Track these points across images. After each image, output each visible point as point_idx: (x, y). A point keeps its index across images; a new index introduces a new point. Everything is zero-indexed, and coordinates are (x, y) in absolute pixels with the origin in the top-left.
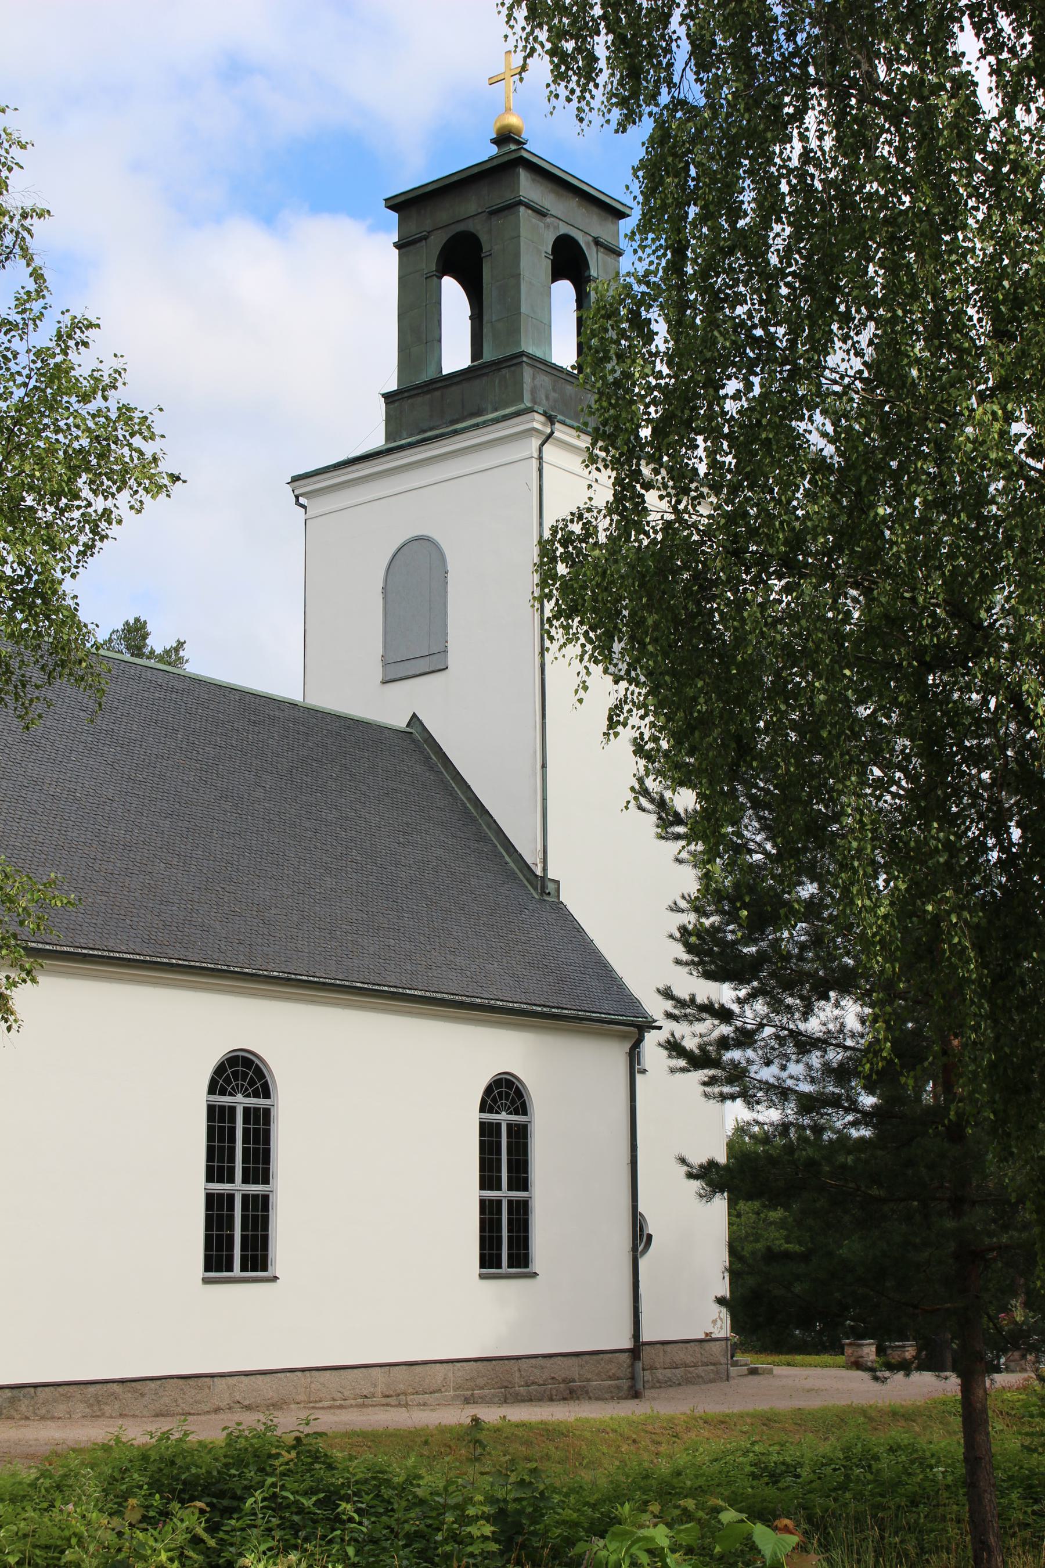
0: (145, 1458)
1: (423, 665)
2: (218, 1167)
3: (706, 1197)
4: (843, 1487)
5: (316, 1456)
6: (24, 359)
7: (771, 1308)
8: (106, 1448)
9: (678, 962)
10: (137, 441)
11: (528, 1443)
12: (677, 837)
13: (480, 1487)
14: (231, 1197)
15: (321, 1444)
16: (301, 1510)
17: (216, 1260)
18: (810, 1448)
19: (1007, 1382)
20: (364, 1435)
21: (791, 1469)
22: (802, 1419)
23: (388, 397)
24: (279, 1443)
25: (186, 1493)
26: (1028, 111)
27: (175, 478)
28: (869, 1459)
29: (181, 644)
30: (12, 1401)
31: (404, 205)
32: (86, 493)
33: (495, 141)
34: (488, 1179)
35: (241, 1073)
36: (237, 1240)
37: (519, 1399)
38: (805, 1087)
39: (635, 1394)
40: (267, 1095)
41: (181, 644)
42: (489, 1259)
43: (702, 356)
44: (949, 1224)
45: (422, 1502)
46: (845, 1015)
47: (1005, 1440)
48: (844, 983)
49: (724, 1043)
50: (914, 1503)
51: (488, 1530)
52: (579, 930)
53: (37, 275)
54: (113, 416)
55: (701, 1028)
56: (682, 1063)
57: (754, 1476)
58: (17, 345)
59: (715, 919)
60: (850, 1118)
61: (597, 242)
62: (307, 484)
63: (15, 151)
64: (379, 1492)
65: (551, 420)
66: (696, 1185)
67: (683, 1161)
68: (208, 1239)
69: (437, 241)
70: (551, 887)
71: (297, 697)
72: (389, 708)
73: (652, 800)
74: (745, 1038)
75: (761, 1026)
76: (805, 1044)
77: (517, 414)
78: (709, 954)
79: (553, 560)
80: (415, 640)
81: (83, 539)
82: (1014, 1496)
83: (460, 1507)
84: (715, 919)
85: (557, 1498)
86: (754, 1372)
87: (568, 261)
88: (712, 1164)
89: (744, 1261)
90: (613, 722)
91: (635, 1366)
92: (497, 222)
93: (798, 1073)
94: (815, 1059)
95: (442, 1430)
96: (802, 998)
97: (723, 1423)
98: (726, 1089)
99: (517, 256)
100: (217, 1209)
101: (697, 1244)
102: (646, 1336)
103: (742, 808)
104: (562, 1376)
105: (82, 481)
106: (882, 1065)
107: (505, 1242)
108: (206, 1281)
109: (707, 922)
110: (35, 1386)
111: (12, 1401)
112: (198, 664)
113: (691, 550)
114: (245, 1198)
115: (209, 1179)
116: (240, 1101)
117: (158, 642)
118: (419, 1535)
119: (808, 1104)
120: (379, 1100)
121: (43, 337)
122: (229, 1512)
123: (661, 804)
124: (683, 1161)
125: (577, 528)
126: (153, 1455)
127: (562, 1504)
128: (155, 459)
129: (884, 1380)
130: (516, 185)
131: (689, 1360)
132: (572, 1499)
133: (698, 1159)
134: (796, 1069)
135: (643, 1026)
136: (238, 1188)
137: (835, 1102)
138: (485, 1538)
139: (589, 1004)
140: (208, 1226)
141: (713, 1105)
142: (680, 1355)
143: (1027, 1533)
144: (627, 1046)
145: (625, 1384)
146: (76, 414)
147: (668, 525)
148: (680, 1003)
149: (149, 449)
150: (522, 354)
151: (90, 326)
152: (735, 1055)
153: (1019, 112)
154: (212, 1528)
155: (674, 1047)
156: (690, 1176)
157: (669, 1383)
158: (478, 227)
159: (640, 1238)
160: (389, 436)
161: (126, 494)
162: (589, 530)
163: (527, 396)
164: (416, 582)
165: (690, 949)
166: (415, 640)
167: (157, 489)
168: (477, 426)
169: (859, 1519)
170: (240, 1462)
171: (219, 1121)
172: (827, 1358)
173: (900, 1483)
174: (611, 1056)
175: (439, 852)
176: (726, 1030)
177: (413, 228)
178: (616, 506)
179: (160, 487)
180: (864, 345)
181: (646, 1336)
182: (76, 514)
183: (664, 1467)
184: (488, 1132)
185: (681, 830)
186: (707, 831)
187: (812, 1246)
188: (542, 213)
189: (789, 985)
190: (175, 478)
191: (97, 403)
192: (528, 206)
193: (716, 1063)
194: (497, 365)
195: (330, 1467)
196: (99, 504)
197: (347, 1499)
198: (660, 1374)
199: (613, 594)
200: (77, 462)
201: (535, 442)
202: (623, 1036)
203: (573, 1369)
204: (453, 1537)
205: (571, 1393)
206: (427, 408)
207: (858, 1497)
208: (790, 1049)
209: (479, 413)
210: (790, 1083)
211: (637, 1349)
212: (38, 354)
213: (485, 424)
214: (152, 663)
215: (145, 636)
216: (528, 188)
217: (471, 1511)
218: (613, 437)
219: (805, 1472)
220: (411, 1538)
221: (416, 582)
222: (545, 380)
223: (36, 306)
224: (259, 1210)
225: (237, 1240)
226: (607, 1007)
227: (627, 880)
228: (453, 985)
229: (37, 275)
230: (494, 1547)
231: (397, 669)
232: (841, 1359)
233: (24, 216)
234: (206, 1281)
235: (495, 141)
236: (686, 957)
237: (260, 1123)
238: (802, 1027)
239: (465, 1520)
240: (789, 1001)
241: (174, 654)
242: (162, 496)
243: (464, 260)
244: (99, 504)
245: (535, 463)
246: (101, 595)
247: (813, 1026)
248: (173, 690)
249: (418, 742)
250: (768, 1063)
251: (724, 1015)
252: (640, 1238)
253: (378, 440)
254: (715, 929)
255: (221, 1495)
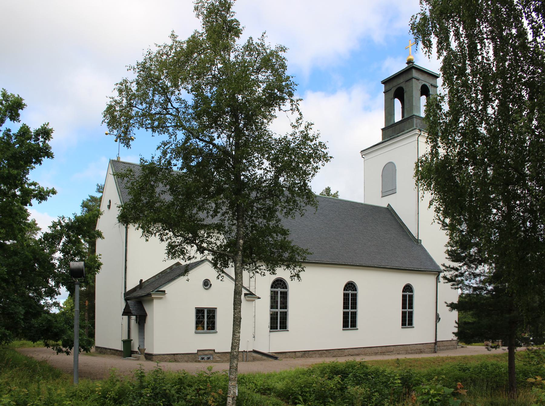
0: (329, 366)
1: (391, 192)
2: (346, 306)
3: (451, 311)
4: (480, 373)
5: (364, 366)
6: (298, 134)
7: (465, 334)
8: (321, 364)
9: (446, 258)
10: (323, 150)
11: (410, 363)
12: (447, 229)
13: (398, 372)
14: (348, 312)
15: (365, 364)
16: (360, 377)
17: (345, 325)
18: (473, 364)
19: (521, 350)
20: (376, 361)
21: (468, 369)
22: (472, 357)
23: (383, 130)
24: (356, 363)
25: (337, 373)
26: (540, 38)
27: (331, 157)
28: (486, 367)
29: (338, 192)
30: (304, 354)
31: (385, 82)
32: (312, 163)
33: (407, 63)
34: (404, 307)
35: (350, 286)
36: (350, 321)
37: (409, 353)
38: (475, 285)
39: (435, 352)
40: (356, 290)
41: (338, 192)
42: (404, 324)
43: (456, 110)
44: (507, 316)
45: (386, 376)
46: (484, 268)
47: (518, 363)
48: (485, 261)
49: (456, 276)
50: (496, 376)
51: (399, 381)
52: (426, 251)
53: (301, 114)
54: (318, 144)
55: (451, 273)
56: (446, 281)
57: (460, 370)
58: (297, 131)
59: (455, 248)
60: (485, 292)
61: (432, 85)
62: (365, 152)
63: (295, 86)
64: (377, 373)
65: (420, 131)
66: (449, 308)
67: (446, 303)
68: (344, 321)
69: (393, 90)
70: (419, 241)
71: (362, 202)
72: (383, 203)
73: (441, 221)
74: (462, 275)
75: (465, 272)
76: (475, 276)
77: (412, 130)
78: (454, 256)
79: (418, 167)
80: (389, 188)
81: (312, 173)
82: (521, 375)
83: (393, 377)
84: (455, 248)
85: (415, 375)
86: (462, 347)
87: (425, 91)
88: (452, 303)
89: (461, 324)
90: (431, 204)
91: (436, 346)
92: (408, 83)
93: (474, 283)
94: (478, 279)
95: (392, 360)
96: (475, 265)
97: (454, 358)
98: (456, 287)
99: (412, 91)
100: (345, 315)
101: (450, 321)
102: (438, 340)
103: (463, 222)
104: (419, 348)
105: (311, 160)
106: (493, 279)
107: (407, 320)
108: (343, 330)
109: (453, 249)
110: (309, 351)
111: (304, 354)
112: (341, 197)
113: (450, 163)
114: (351, 312)
115: (344, 309)
116: (350, 292)
117: (333, 192)
118: (385, 382)
119: (475, 289)
120: (380, 291)
121: (302, 128)
122: (346, 377)
123: (443, 222)
124: (446, 303)
125: (424, 159)
126: (331, 366)
127: (416, 376)
128: (327, 153)
129: (490, 350)
130: (412, 74)
131: (448, 345)
132: (419, 375)
133: (449, 302)
134: (473, 281)
135: (439, 272)
136: (350, 310)
137: (482, 288)
138: (399, 383)
139: (428, 268)
140: (344, 318)
141: (454, 290)
142: (445, 344)
143: (523, 383)
144: (436, 277)
145: (433, 350)
146: (310, 145)
147: (445, 156)
148: (447, 267)
149: (325, 151)
150: (414, 115)
151: (312, 124)
152: (459, 279)
153: (538, 38)
154: (342, 380)
155: (445, 278)
156: (447, 306)
157: (443, 350)
158: (403, 85)
159: (438, 319)
160: (383, 139)
161: (321, 162)
162: (427, 158)
163: (415, 125)
164: (389, 171)
165: (449, 255)
166: (389, 188)
167: (327, 160)
168: (403, 134)
169: (483, 380)
170: (348, 367)
171: (346, 296)
172: (480, 344)
173: (493, 372)
174: (433, 279)
175: (394, 235)
176: (457, 273)
177: (388, 88)
178: (431, 153)
179: (328, 160)
180: (495, 106)
181: (438, 340)
182: (311, 167)
183: (439, 369)
184: (404, 297)
185: (447, 228)
186: (452, 228)
187: (478, 318)
188: (418, 80)
189: (472, 262)
190: (331, 157)
191: (314, 142)
192: (415, 78)
193: (454, 281)
194: (408, 119)
195: (367, 368)
196: (315, 165)
197: (370, 375)
198: (441, 348)
199: (433, 174)
200: (310, 156)
201: (417, 137)
202: (435, 274)
203: (421, 347)
204: (392, 383)
205: (421, 352)
206: (392, 131)
207: (483, 375)
208: (472, 277)
209: (403, 131)
210: (471, 285)
211: (436, 343)
212: (301, 132)
213: (405, 133)
214: (330, 197)
215: (330, 191)
216: (415, 74)
217: (396, 378)
218: (433, 137)
219: (471, 370)
220: (383, 383)
221: (389, 171)
222: (419, 121)
223: (300, 121)
224: (354, 315)
225: (350, 321)
226: (432, 268)
227: (435, 239)
228: (397, 265)
229: (301, 114)
230: (401, 385)
231: (385, 194)
232: (483, 344)
233: (297, 101)
234: (343, 330)
235: (407, 63)
236: (448, 257)
237: (355, 297)
238: (475, 271)
239: (394, 379)
240: (472, 266)
241: (336, 195)
242: (329, 162)
243: (400, 94)
244: (315, 165)
245: (416, 142)
246: (316, 185)
247: (477, 271)
248: (336, 203)
249: (389, 210)
250: (467, 280)
251: (457, 270)
252: (438, 319)
253: (380, 140)
254: (455, 251)
255: (344, 374)
